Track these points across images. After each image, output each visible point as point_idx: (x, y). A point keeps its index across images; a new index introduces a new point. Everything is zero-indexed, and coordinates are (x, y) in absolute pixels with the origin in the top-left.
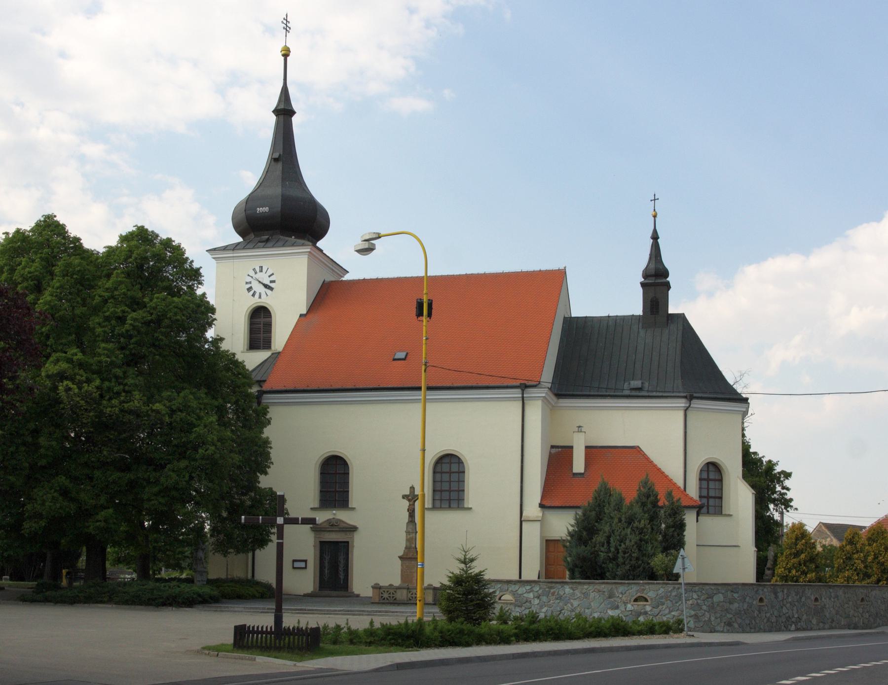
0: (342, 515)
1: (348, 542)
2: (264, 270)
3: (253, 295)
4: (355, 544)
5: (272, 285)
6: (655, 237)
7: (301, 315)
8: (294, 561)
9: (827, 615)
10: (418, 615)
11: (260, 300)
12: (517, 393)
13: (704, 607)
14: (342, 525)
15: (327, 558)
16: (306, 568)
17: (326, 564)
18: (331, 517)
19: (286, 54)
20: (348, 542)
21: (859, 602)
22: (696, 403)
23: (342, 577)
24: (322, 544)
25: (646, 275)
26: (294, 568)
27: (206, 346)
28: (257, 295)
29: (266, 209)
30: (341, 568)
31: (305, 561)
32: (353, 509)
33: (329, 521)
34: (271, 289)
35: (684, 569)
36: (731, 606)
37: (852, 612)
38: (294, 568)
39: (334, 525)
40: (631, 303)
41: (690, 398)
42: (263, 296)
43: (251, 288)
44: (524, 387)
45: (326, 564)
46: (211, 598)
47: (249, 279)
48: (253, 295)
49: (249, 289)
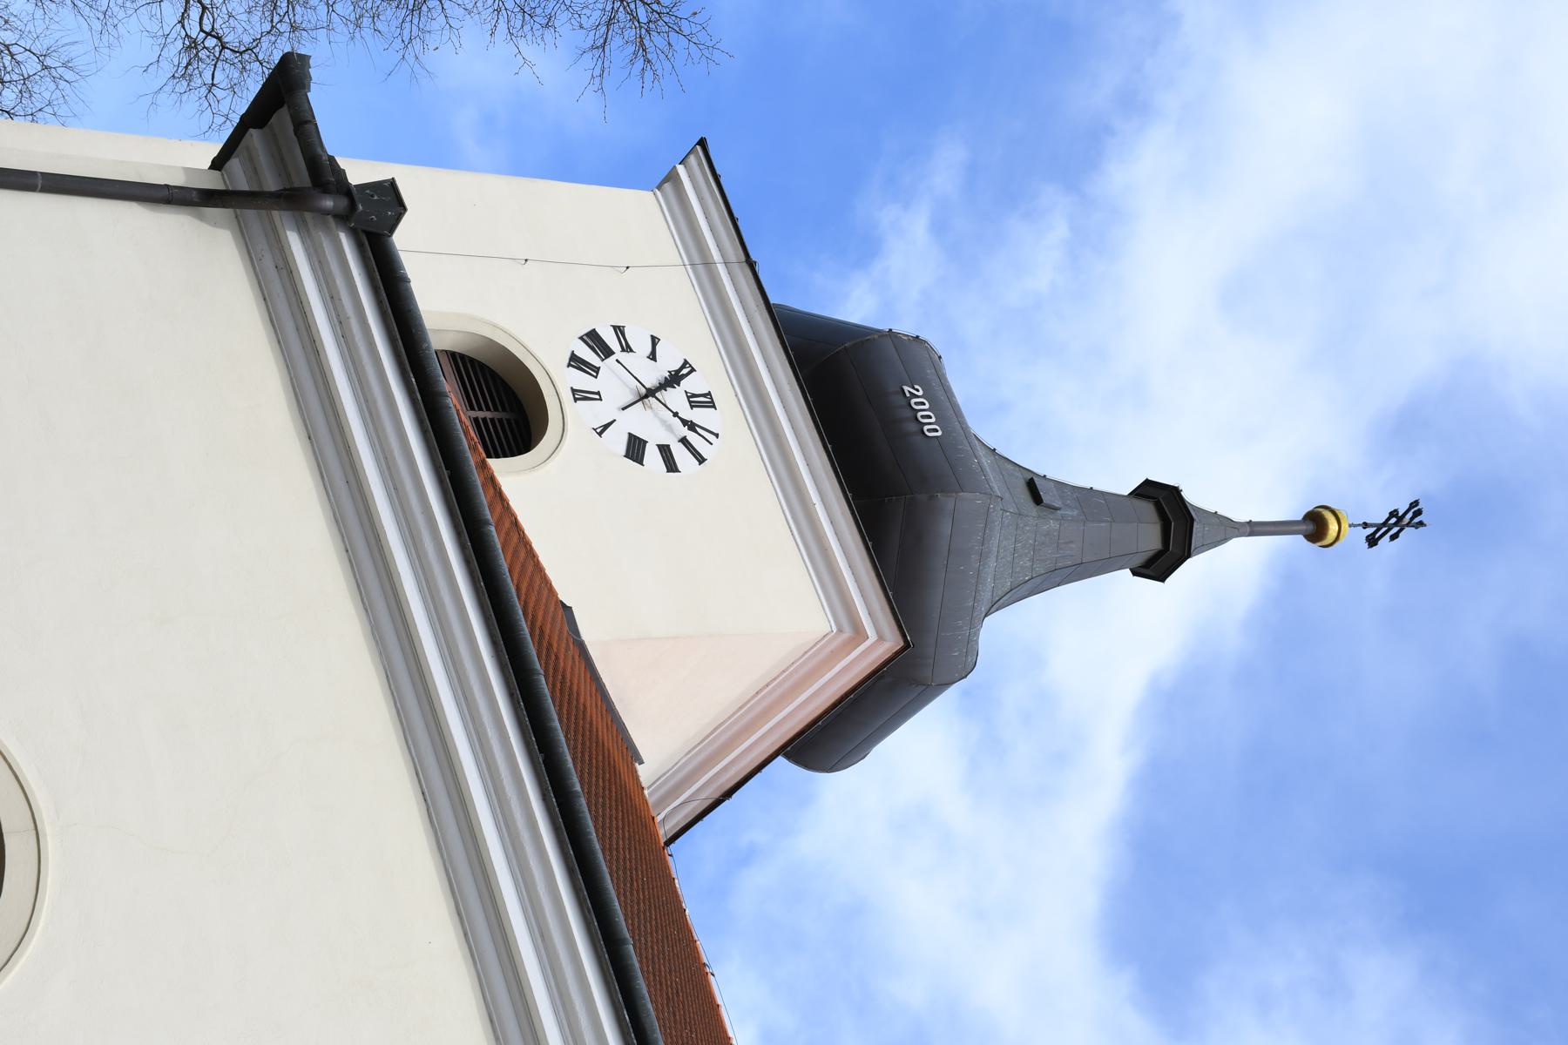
3: (576, 361)
11: (711, 375)
29: (932, 428)
34: (635, 448)
43: (607, 352)
48: (576, 361)
49: (593, 339)
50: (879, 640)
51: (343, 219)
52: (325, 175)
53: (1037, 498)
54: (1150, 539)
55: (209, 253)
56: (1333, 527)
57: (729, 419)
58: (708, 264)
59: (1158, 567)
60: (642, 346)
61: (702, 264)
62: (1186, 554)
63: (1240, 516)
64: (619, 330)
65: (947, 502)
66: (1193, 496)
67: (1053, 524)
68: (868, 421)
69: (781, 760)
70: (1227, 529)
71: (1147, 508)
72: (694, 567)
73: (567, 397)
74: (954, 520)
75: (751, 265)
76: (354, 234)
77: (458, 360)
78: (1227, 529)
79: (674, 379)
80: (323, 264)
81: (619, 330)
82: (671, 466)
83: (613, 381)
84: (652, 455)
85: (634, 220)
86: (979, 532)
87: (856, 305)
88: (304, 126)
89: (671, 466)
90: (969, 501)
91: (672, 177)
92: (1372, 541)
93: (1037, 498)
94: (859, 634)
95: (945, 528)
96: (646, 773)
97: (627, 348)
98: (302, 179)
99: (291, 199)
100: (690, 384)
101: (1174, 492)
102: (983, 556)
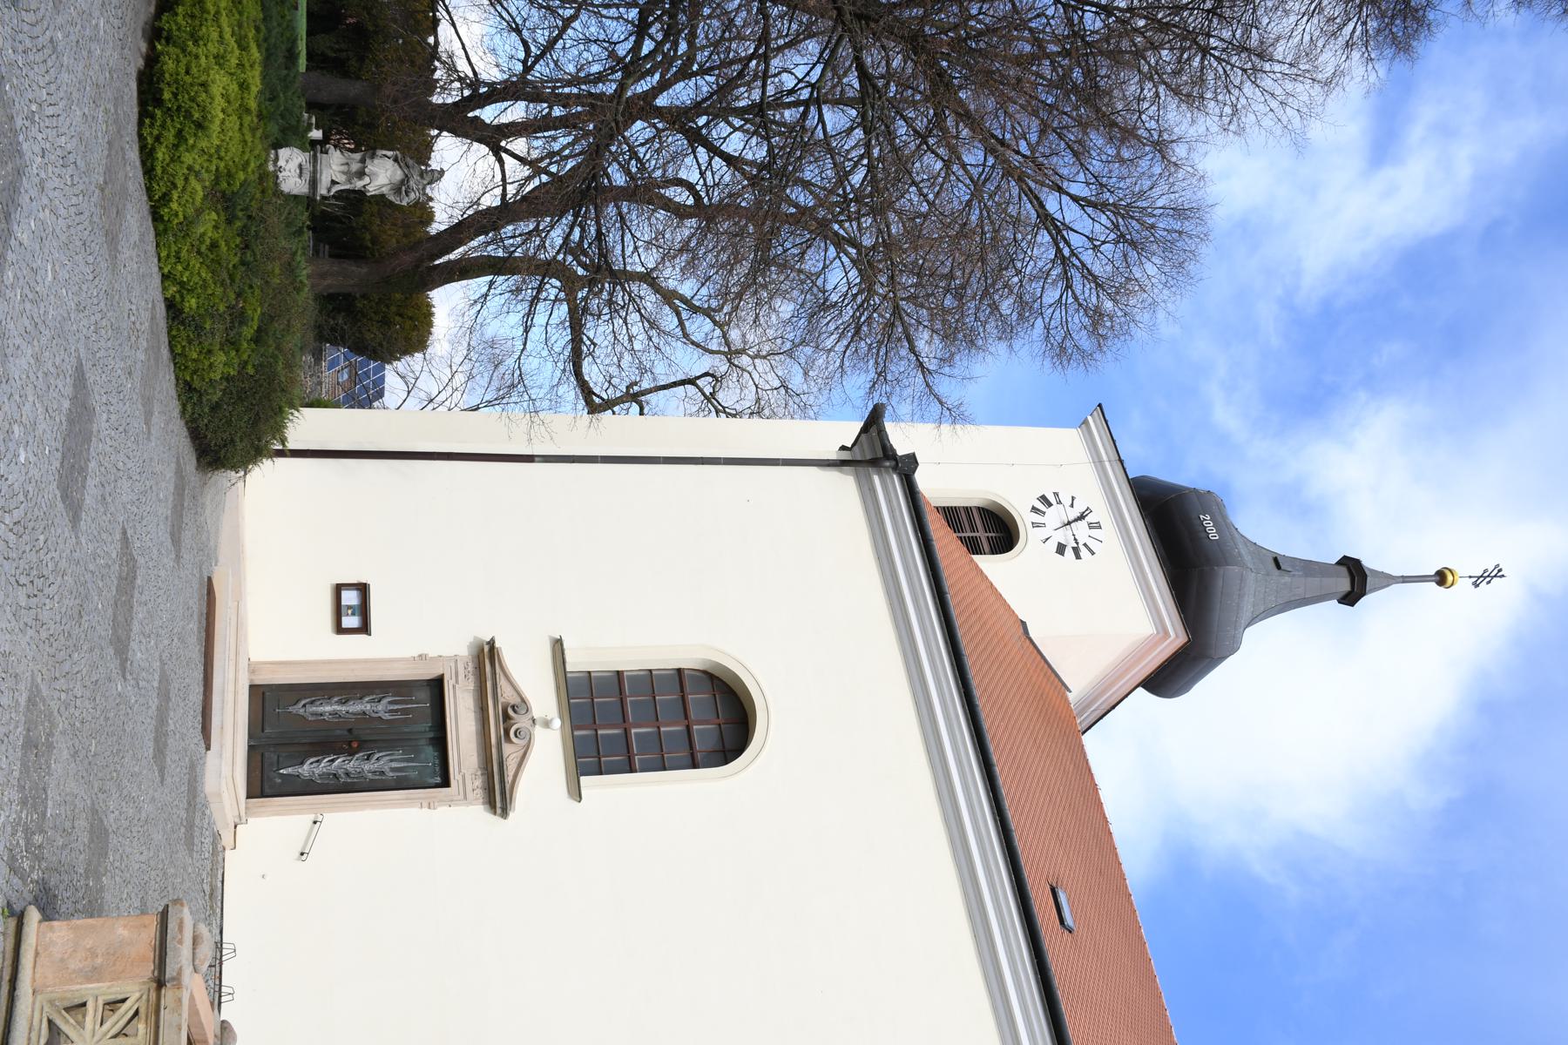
0: (545, 753)
1: (446, 783)
2: (1094, 532)
3: (1035, 510)
4: (442, 810)
5: (1084, 552)
7: (1024, 623)
8: (363, 589)
10: (199, 188)
11: (1101, 513)
14: (511, 752)
15: (383, 708)
16: (340, 630)
17: (355, 707)
18: (537, 712)
19: (1441, 578)
20: (446, 783)
23: (307, 769)
24: (436, 686)
26: (339, 589)
27: (398, 296)
28: (1037, 518)
29: (1213, 535)
30: (340, 764)
31: (364, 628)
33: (522, 705)
34: (1061, 549)
35: (160, 983)
38: (339, 589)
39: (503, 721)
42: (1041, 533)
43: (1050, 505)
45: (355, 707)
46: (153, 169)
47: (1067, 501)
48: (1035, 510)
49: (1043, 499)
50: (1176, 636)
51: (895, 468)
52: (888, 453)
53: (1278, 567)
54: (1344, 585)
55: (844, 485)
56: (1450, 578)
57: (1109, 532)
58: (1101, 462)
59: (1350, 599)
60: (1067, 501)
61: (1098, 462)
62: (1363, 594)
63: (1396, 572)
64: (1056, 494)
65: (1221, 571)
66: (1367, 563)
67: (1287, 579)
68: (1180, 534)
69: (1140, 689)
70: (1388, 580)
71: (1344, 570)
72: (1084, 599)
73: (354, 647)
74: (1227, 576)
75: (1121, 462)
76: (900, 475)
77: (952, 516)
78: (1388, 580)
79: (1082, 517)
80: (887, 486)
81: (1056, 494)
82: (1078, 557)
83: (1054, 516)
84: (1069, 552)
85: (1068, 442)
86: (1240, 585)
87: (1181, 474)
88: (882, 433)
89: (1078, 557)
90: (1233, 570)
91: (1085, 422)
92: (1476, 585)
93: (1278, 567)
94: (1166, 634)
95: (1220, 583)
96: (1072, 697)
97: (1060, 502)
98: (880, 454)
99: (874, 463)
100: (1089, 519)
101: (1357, 562)
102: (1241, 596)
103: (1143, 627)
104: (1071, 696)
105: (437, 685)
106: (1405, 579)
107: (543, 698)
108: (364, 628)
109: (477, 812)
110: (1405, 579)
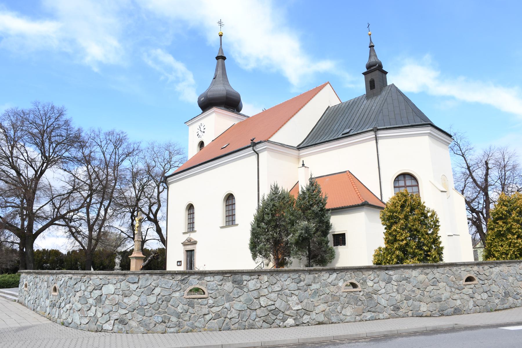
5: (204, 130)
6: (371, 47)
8: (178, 262)
9: (383, 302)
11: (199, 123)
12: (250, 150)
13: (91, 301)
15: (188, 259)
16: (181, 265)
19: (221, 36)
21: (463, 282)
22: (380, 134)
25: (369, 67)
29: (203, 99)
31: (181, 262)
32: (237, 225)
34: (204, 132)
36: (126, 300)
37: (446, 295)
40: (359, 87)
41: (376, 130)
44: (254, 144)
54: (220, 60)
55: (171, 187)
57: (202, 122)
59: (224, 58)
70: (221, 49)
73: (182, 262)
78: (221, 49)
80: (169, 180)
103: (214, 115)
104: (236, 123)
105: (187, 251)
106: (221, 44)
107: (187, 236)
108: (181, 262)
109: (197, 246)
110: (221, 44)
